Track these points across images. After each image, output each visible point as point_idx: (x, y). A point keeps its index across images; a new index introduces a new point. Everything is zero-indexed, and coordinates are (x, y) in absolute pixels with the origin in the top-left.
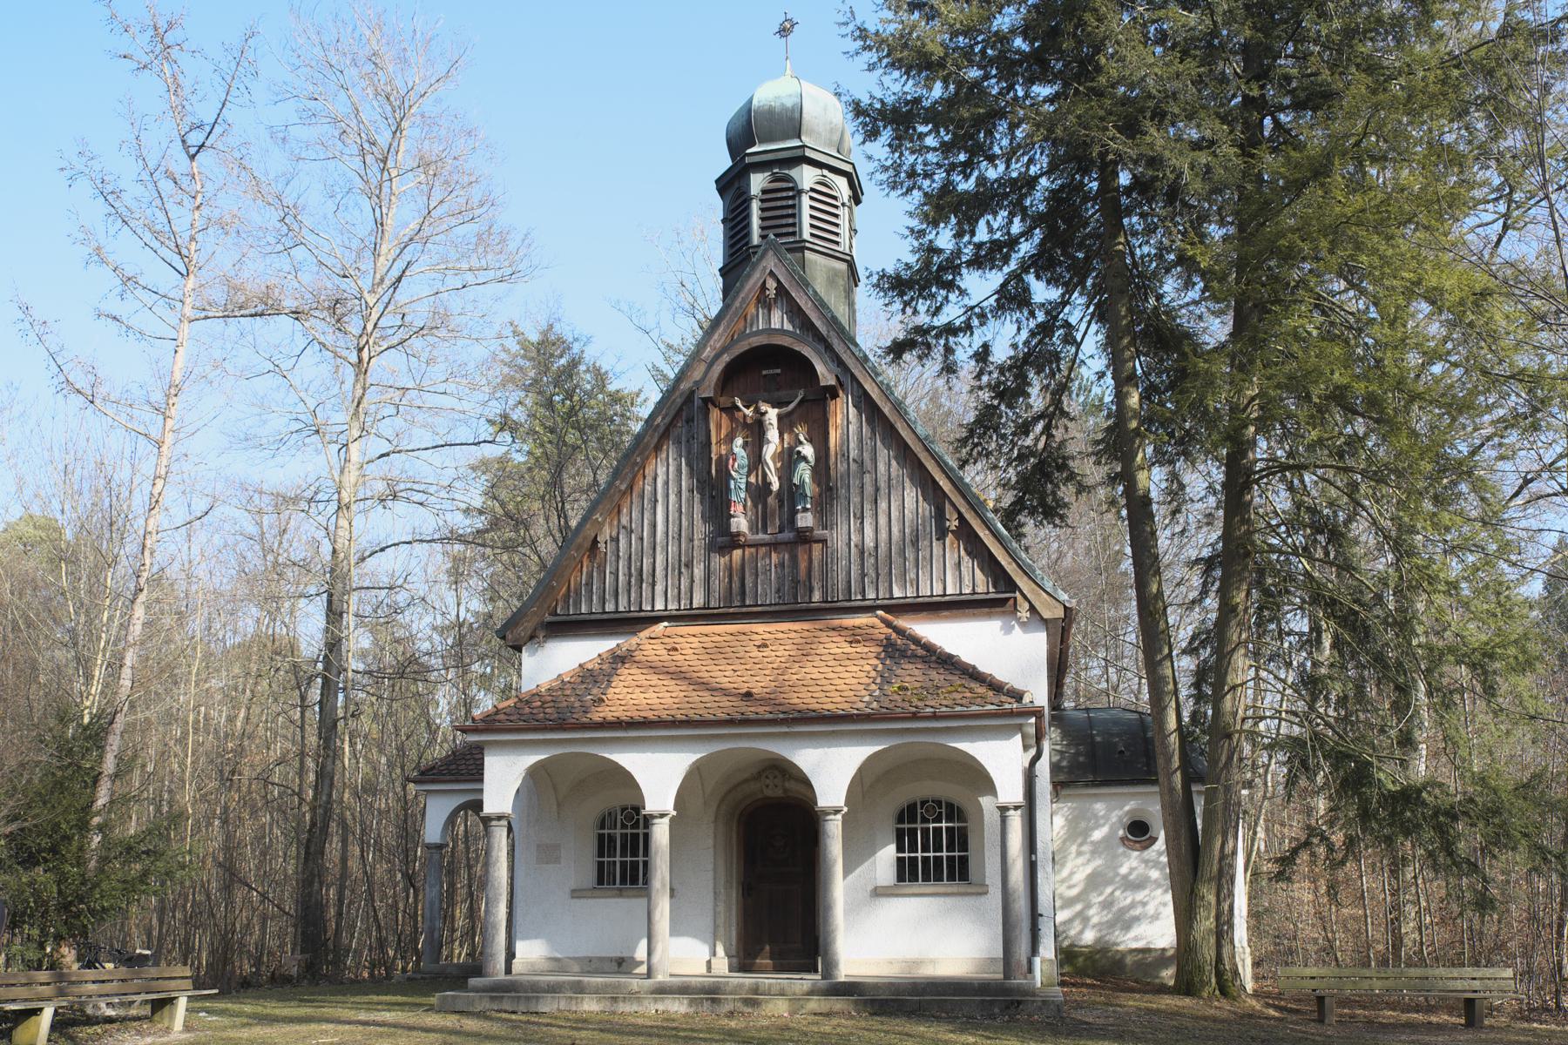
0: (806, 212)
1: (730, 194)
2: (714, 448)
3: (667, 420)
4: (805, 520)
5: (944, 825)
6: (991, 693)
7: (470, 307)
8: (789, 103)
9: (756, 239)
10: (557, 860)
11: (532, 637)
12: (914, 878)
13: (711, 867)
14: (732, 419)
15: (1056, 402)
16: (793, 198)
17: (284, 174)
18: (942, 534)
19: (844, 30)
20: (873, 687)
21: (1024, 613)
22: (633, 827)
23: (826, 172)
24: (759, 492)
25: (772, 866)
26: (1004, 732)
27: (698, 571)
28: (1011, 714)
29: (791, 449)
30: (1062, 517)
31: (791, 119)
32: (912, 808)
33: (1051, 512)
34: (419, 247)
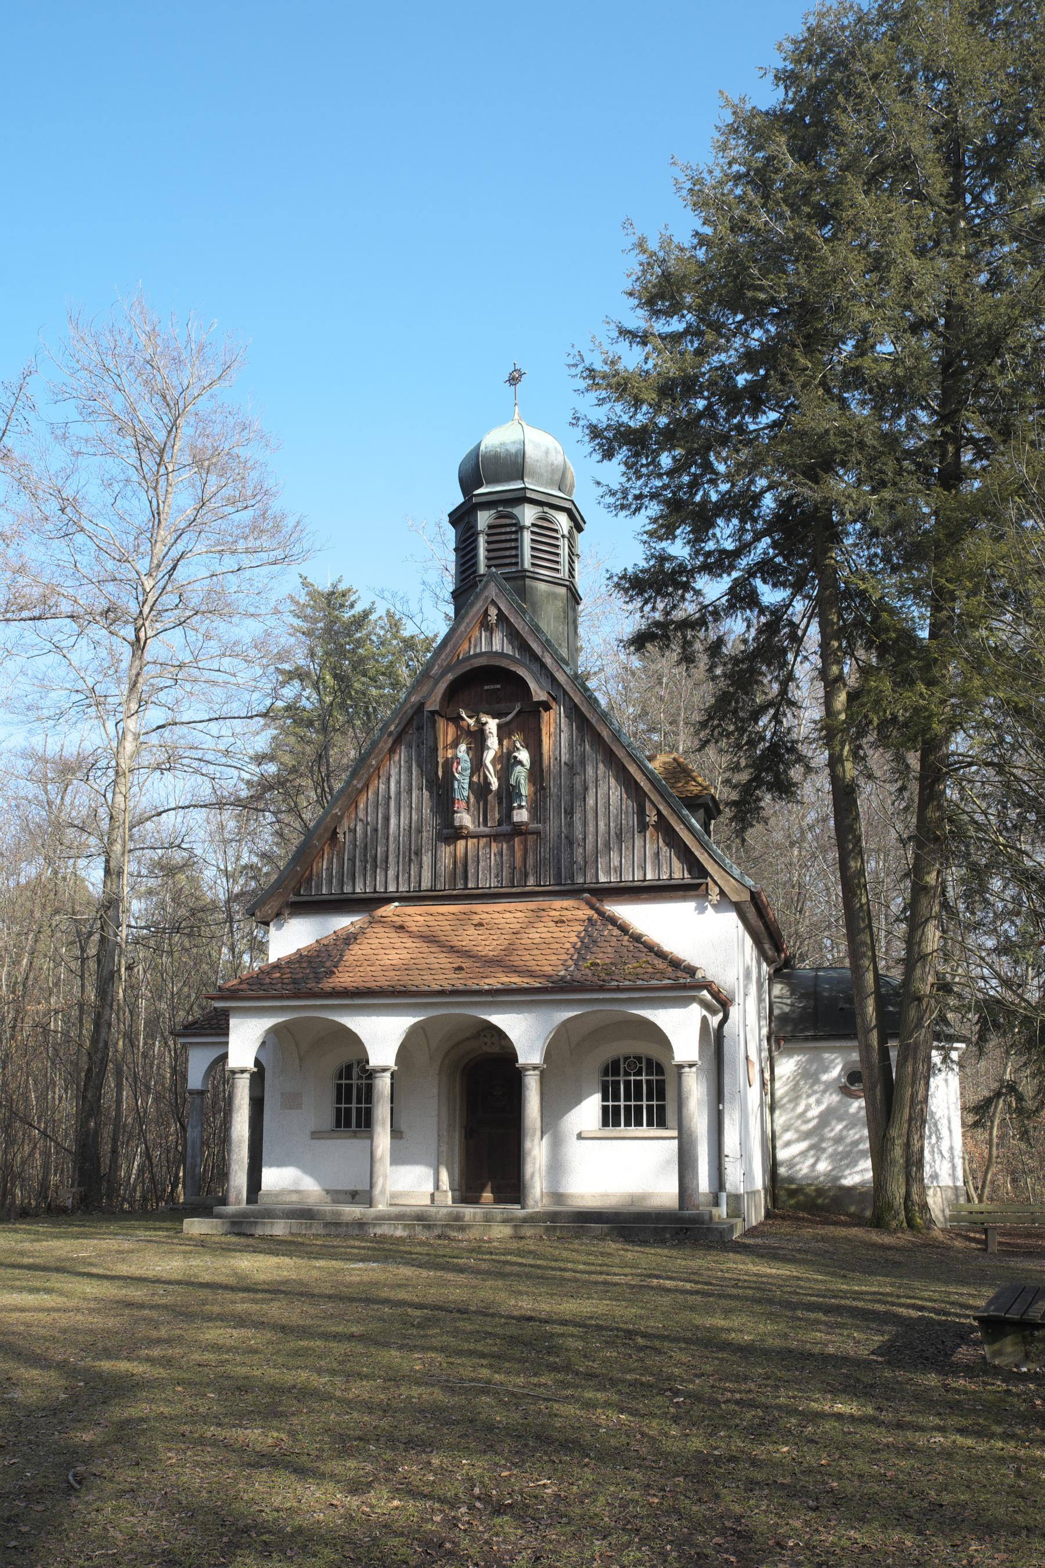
0: (527, 552)
1: (462, 526)
2: (440, 752)
3: (399, 729)
4: (522, 816)
5: (644, 1078)
6: (670, 969)
7: (245, 586)
8: (513, 449)
9: (482, 569)
10: (299, 1106)
11: (278, 915)
12: (348, 1124)
13: (435, 1113)
14: (458, 727)
15: (783, 691)
16: (516, 532)
17: (63, 469)
18: (643, 827)
19: (574, 371)
20: (570, 962)
21: (715, 897)
22: (635, 1075)
23: (546, 509)
24: (481, 790)
25: (483, 1111)
26: (684, 1002)
27: (427, 859)
28: (685, 987)
29: (510, 753)
30: (794, 793)
31: (516, 463)
32: (615, 1064)
33: (785, 789)
34: (194, 536)
